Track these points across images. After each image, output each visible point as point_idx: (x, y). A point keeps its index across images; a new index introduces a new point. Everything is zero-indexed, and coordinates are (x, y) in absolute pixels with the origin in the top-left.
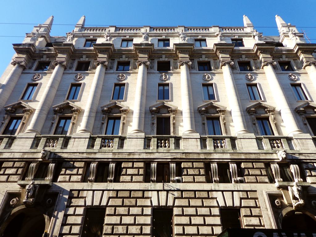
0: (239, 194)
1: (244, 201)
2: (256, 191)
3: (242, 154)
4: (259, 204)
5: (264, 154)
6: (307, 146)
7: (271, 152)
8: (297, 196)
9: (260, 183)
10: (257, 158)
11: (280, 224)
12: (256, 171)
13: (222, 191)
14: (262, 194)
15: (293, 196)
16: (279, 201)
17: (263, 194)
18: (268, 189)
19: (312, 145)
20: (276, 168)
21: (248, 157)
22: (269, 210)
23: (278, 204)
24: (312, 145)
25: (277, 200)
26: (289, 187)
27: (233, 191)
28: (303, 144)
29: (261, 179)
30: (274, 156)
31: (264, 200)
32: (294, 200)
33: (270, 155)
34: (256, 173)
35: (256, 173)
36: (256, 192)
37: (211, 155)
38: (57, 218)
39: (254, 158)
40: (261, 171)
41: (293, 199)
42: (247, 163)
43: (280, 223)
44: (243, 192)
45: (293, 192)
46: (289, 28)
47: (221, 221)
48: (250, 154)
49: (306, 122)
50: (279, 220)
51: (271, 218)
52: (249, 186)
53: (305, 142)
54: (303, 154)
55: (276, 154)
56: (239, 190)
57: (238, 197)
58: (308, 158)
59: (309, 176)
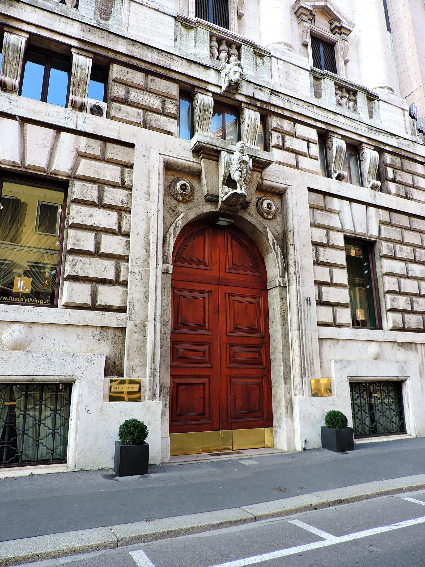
0: (77, 142)
1: (85, 164)
2: (132, 146)
3: (121, 39)
4: (131, 181)
5: (184, 61)
6: (295, 82)
7: (206, 62)
8: (236, 176)
9: (152, 128)
10: (161, 64)
11: (172, 236)
12: (148, 98)
13: (24, 120)
14: (146, 158)
15: (225, 176)
16: (187, 184)
17: (149, 157)
18: (166, 149)
19: (307, 84)
20: (202, 103)
21: (138, 52)
22: (154, 198)
23: (182, 189)
24: (307, 84)
25: (183, 182)
26: (223, 154)
27: (59, 129)
28: (287, 74)
29: (158, 120)
30: (210, 76)
31: (147, 173)
32: (226, 187)
33: (202, 69)
34: (147, 101)
35: (147, 101)
36: (130, 149)
37: (11, 5)
38: (408, 393)
39: (155, 61)
40: (163, 103)
41: (223, 184)
42: (131, 71)
43: (174, 234)
44: (92, 141)
45: (228, 167)
46: (314, 210)
47: (405, 424)
48: (145, 47)
49: (309, 40)
50: (172, 228)
51: (152, 219)
52: (117, 128)
53: (292, 73)
54: (281, 95)
55: (217, 72)
56: (79, 129)
57: (72, 148)
58: (287, 106)
59: (277, 147)
